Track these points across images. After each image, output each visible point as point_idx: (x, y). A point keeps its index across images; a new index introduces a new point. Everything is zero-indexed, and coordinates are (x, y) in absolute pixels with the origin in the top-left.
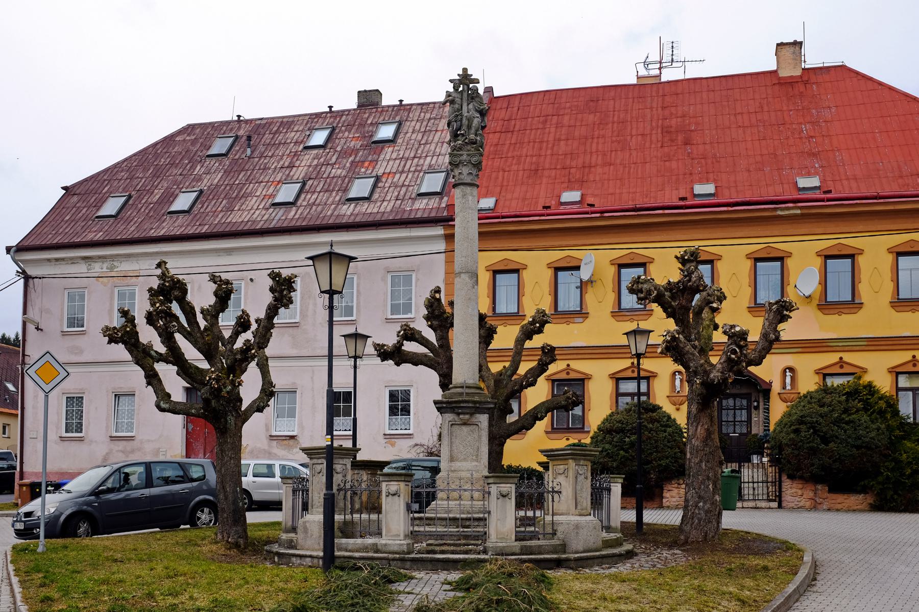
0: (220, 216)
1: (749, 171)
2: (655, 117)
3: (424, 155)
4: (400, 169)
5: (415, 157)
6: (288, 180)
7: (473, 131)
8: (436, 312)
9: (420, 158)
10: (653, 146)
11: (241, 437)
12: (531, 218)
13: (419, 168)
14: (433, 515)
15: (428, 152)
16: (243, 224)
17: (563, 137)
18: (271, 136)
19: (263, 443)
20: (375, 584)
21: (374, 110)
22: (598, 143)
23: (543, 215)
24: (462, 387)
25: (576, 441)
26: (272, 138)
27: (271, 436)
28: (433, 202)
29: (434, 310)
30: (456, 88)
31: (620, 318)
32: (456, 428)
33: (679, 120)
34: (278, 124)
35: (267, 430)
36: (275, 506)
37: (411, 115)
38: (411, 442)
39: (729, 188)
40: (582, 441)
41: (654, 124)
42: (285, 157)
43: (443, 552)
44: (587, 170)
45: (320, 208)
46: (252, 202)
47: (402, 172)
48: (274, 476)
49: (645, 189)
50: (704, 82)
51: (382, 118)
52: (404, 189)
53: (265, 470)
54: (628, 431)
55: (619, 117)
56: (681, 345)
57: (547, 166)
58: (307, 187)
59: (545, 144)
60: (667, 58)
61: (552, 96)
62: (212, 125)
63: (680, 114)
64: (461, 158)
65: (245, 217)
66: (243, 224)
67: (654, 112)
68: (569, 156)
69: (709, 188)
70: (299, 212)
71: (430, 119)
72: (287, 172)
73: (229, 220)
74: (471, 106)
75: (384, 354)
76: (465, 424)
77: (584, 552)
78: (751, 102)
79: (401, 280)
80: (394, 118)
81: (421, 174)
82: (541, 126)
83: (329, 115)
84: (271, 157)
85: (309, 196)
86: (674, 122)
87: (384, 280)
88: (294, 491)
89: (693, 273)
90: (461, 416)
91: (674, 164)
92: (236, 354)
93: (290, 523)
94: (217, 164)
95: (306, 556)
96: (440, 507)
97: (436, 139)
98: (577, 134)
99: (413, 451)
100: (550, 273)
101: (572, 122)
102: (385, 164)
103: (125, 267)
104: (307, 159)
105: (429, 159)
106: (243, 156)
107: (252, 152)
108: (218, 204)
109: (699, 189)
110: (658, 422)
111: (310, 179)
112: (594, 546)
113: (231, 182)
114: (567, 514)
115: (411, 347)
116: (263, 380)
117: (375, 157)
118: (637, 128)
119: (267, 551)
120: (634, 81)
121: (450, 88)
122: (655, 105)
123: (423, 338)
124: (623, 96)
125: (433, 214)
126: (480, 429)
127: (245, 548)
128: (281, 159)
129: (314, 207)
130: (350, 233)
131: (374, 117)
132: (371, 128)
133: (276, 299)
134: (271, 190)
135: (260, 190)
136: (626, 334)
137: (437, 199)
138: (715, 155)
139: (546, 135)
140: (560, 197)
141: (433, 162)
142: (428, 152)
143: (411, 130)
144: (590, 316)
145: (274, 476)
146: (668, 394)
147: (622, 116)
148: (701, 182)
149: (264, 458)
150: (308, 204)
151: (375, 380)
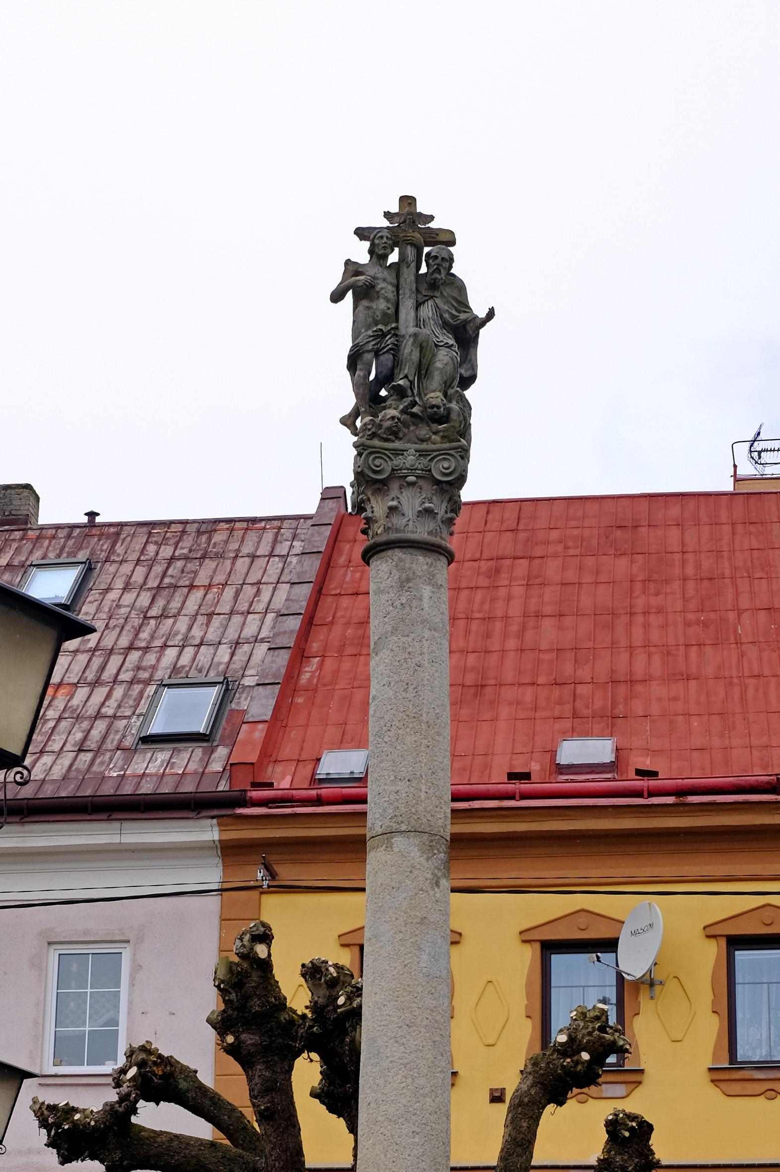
3: (158, 643)
4: (90, 676)
5: (131, 648)
8: (256, 1005)
9: (146, 649)
12: (477, 804)
15: (169, 637)
17: (548, 610)
21: (18, 535)
22: (646, 626)
23: (511, 796)
28: (187, 760)
29: (246, 998)
30: (378, 255)
31: (737, 1088)
37: (119, 549)
44: (622, 689)
47: (96, 683)
51: (38, 554)
55: (698, 566)
57: (509, 676)
59: (498, 625)
61: (510, 514)
64: (398, 461)
68: (570, 655)
71: (172, 559)
74: (427, 311)
81: (151, 690)
82: (484, 582)
87: (37, 964)
97: (192, 605)
98: (586, 601)
100: (529, 955)
105: (171, 654)
118: (752, 594)
121: (361, 253)
125: (188, 787)
131: (18, 551)
137: (199, 753)
140: (553, 753)
141: (185, 660)
143: (119, 584)
144: (646, 1079)
147: (706, 563)
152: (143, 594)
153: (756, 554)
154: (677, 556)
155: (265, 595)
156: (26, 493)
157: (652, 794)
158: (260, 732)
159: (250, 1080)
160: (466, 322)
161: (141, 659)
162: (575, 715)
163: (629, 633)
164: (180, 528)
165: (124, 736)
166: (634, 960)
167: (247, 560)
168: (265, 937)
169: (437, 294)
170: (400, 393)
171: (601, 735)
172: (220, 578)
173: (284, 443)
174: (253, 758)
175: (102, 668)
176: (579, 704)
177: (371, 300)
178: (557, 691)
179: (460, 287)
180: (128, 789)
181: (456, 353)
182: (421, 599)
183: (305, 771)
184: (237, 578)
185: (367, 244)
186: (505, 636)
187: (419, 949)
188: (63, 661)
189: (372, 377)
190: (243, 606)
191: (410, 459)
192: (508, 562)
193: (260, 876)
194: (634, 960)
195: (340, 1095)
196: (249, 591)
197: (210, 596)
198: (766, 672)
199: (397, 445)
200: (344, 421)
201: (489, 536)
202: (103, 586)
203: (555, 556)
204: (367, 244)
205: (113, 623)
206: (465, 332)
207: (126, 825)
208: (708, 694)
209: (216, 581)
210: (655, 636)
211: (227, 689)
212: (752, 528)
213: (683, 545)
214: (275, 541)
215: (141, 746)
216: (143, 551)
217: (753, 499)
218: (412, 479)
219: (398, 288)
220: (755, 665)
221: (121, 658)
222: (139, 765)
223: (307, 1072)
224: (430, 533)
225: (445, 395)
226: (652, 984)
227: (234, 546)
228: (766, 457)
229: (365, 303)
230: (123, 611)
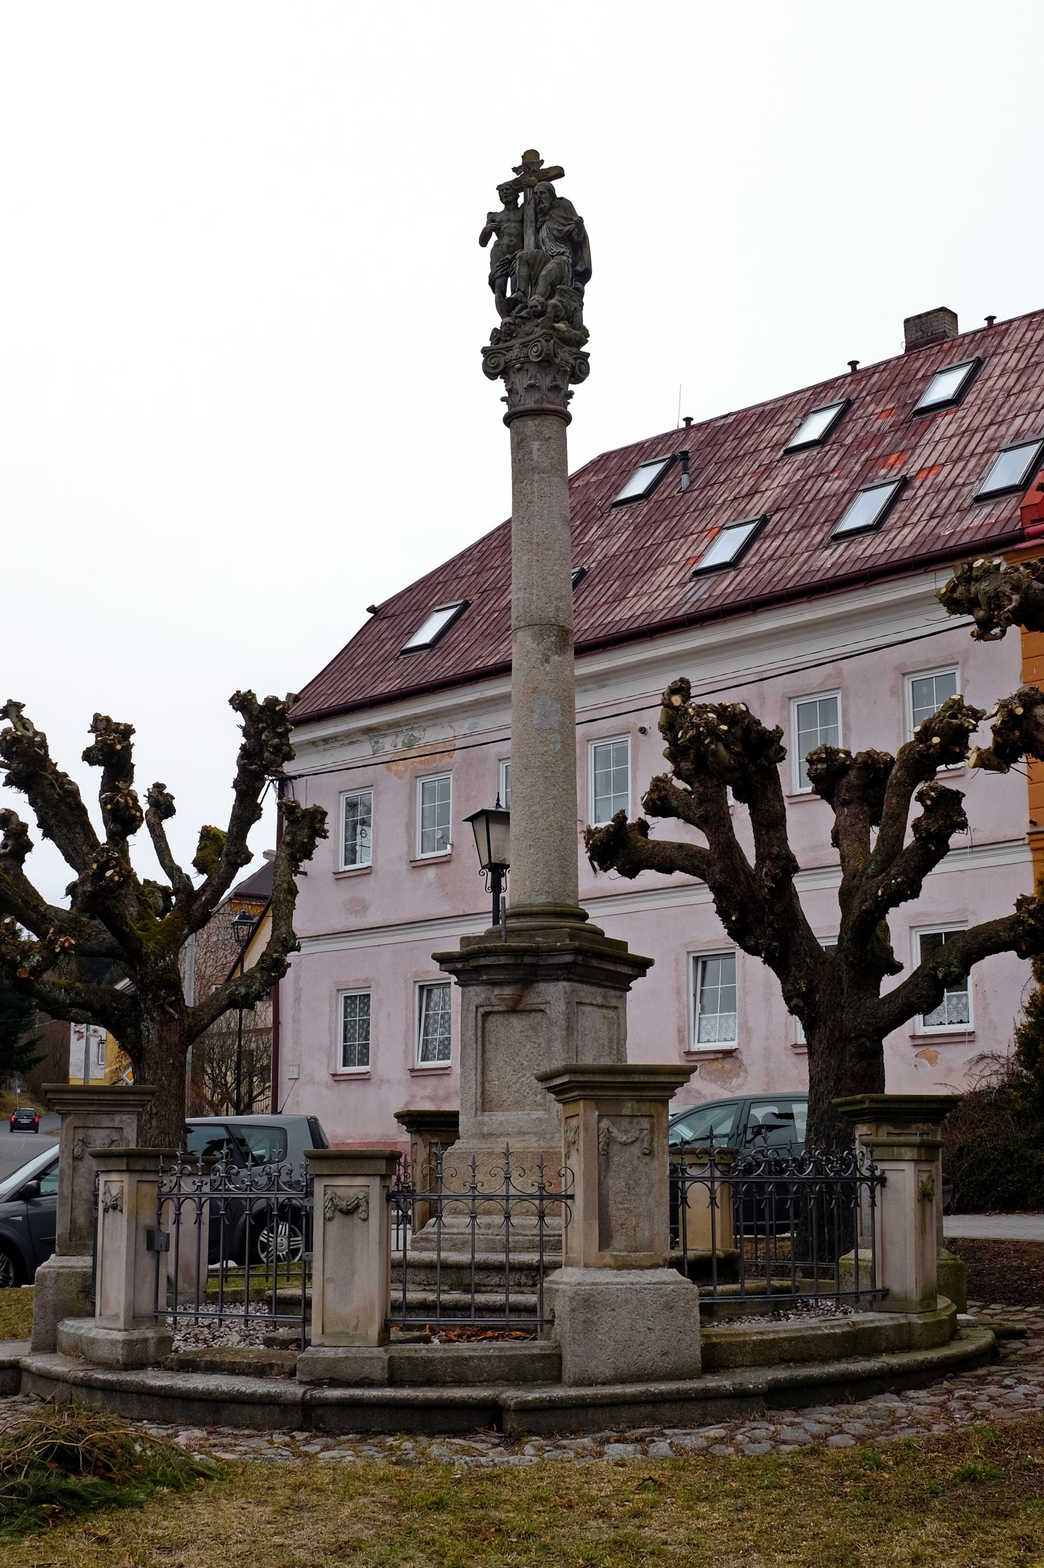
7: (541, 286)
15: (1021, 407)
18: (735, 443)
32: (495, 1024)
35: (681, 1041)
37: (1005, 343)
38: (971, 1052)
46: (664, 575)
70: (739, 578)
77: (621, 1380)
87: (896, 692)
99: (976, 1070)
103: (432, 736)
104: (787, 473)
107: (692, 482)
111: (778, 510)
112: (666, 1364)
130: (815, 603)
142: (1021, 407)
169: (547, 218)
182: (531, 453)
187: (532, 711)
207: (939, 573)
230: (994, 394)
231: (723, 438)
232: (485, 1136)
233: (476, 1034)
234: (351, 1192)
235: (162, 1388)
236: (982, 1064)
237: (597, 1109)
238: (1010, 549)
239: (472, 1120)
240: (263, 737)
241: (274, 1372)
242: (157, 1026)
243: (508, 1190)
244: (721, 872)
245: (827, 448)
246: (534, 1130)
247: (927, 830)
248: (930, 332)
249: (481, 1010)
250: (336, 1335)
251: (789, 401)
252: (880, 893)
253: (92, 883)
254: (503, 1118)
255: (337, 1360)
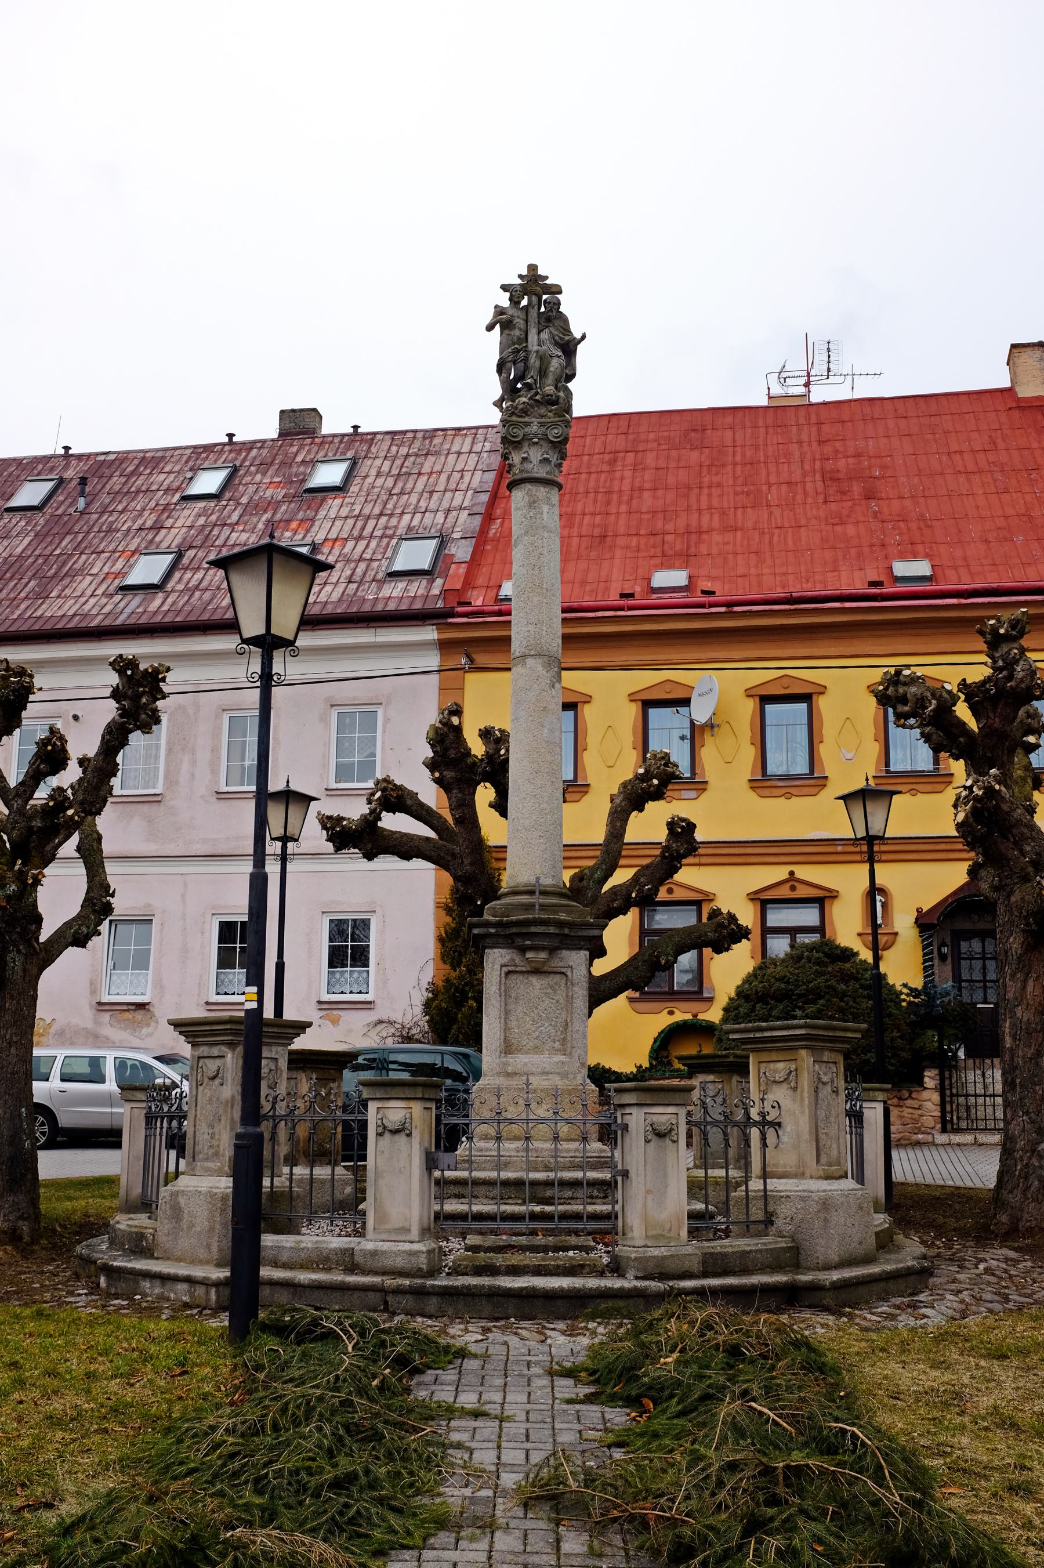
0: (23, 606)
1: (987, 541)
2: (808, 456)
3: (398, 511)
4: (356, 533)
5: (381, 514)
6: (150, 549)
7: (550, 379)
9: (391, 515)
10: (809, 500)
11: (35, 998)
12: (600, 614)
13: (390, 532)
14: (464, 1174)
15: (406, 506)
16: (65, 620)
17: (647, 486)
18: (123, 480)
19: (85, 1017)
20: (381, 1388)
21: (309, 441)
22: (710, 495)
23: (621, 609)
24: (531, 893)
25: (688, 1017)
26: (125, 484)
27: (99, 1003)
28: (417, 588)
29: (446, 750)
30: (514, 301)
31: (766, 792)
32: (516, 980)
33: (851, 460)
34: (136, 462)
35: (93, 992)
36: (106, 1138)
37: (374, 449)
38: (372, 1016)
39: (955, 568)
40: (701, 1017)
41: (807, 467)
42: (146, 513)
43: (515, 1271)
44: (694, 537)
45: (207, 595)
46: (85, 583)
47: (360, 538)
48: (102, 1080)
49: (803, 568)
50: (888, 405)
51: (322, 453)
52: (362, 566)
53: (85, 1069)
54: (800, 996)
55: (744, 455)
56: (1005, 807)
57: (622, 530)
58: (185, 561)
59: (615, 496)
60: (819, 369)
61: (624, 424)
62: (18, 462)
63: (851, 451)
64: (528, 430)
65: (70, 607)
66: (65, 620)
67: (806, 448)
68: (661, 516)
69: (922, 568)
70: (170, 600)
71: (407, 455)
72: (150, 537)
73: (39, 613)
74: (545, 335)
75: (344, 836)
76: (537, 971)
78: (975, 435)
79: (357, 721)
80: (344, 453)
81: (394, 541)
82: (605, 468)
83: (227, 448)
84: (122, 512)
85: (188, 575)
86: (841, 464)
87: (324, 719)
88: (150, 1119)
89: (1017, 662)
90: (530, 955)
91: (851, 530)
92: (31, 818)
93: (137, 1190)
94: (23, 523)
95: (175, 1279)
96: (480, 1153)
97: (420, 487)
98: (671, 480)
99: (373, 1034)
100: (633, 710)
101: (662, 463)
102: (327, 525)
105: (407, 518)
106: (71, 510)
107: (88, 505)
108: (19, 587)
109: (901, 568)
110: (856, 979)
111: (191, 547)
113: (47, 552)
114: (800, 1175)
115: (394, 822)
116: (90, 881)
117: (310, 513)
118: (778, 473)
119: (80, 1257)
120: (764, 402)
121: (504, 300)
122: (804, 437)
123: (422, 805)
124: (748, 424)
125: (417, 605)
126: (569, 983)
127: (34, 1241)
128: (140, 515)
129: (197, 594)
131: (309, 452)
132: (302, 469)
133: (124, 712)
134: (119, 565)
135: (99, 564)
136: (843, 798)
137: (424, 582)
138: (923, 516)
139: (616, 482)
140: (649, 580)
141: (416, 522)
143: (373, 472)
144: (709, 787)
145: (102, 1080)
146: (860, 930)
147: (749, 453)
148: (903, 557)
149: (84, 1045)
150: (186, 589)
151: (322, 885)
152: (389, 479)
153: (781, 446)
154: (730, 449)
155: (467, 479)
156: (313, 414)
157: (711, 606)
158: (462, 570)
159: (449, 799)
160: (569, 341)
161: (388, 521)
162: (664, 555)
163: (699, 501)
164: (410, 435)
165: (377, 572)
166: (701, 711)
167: (455, 456)
168: (458, 711)
170: (528, 387)
171: (680, 568)
172: (437, 468)
173: (471, 396)
174: (459, 586)
175: (363, 528)
176: (666, 547)
177: (511, 330)
178: (652, 539)
179: (565, 320)
180: (379, 607)
181: (562, 361)
183: (492, 594)
184: (448, 468)
185: (508, 294)
186: (619, 503)
188: (315, 589)
189: (512, 377)
190: (452, 486)
191: (535, 428)
192: (622, 455)
193: (463, 661)
194: (701, 711)
195: (501, 806)
196: (456, 476)
197: (431, 480)
198: (786, 525)
199: (527, 419)
200: (495, 404)
201: (610, 437)
202: (363, 474)
203: (652, 450)
204: (508, 294)
205: (369, 498)
206: (569, 347)
207: (379, 630)
208: (748, 540)
209: (435, 470)
210: (715, 502)
211: (442, 541)
212: (779, 430)
213: (734, 441)
214: (473, 443)
215: (388, 579)
216: (388, 451)
217: (779, 411)
218: (536, 440)
219: (527, 321)
220: (779, 521)
221: (375, 521)
222: (387, 591)
223: (485, 794)
224: (547, 473)
225: (556, 388)
226: (712, 727)
227: (446, 446)
228: (789, 381)
229: (507, 332)
230: (376, 490)
231: (107, 472)
232: (508, 1075)
233: (500, 989)
234: (663, 1119)
235: (522, 1289)
236: (379, 1027)
237: (813, 1056)
238: (444, 621)
239: (497, 1061)
240: (144, 700)
241: (585, 1272)
242: (22, 959)
243: (527, 1115)
244: (471, 864)
245: (224, 503)
246: (558, 1071)
247: (677, 851)
248: (299, 424)
249: (505, 969)
250: (656, 1237)
251: (169, 454)
252: (634, 895)
253: (43, 819)
254: (527, 1060)
255: (664, 1258)
